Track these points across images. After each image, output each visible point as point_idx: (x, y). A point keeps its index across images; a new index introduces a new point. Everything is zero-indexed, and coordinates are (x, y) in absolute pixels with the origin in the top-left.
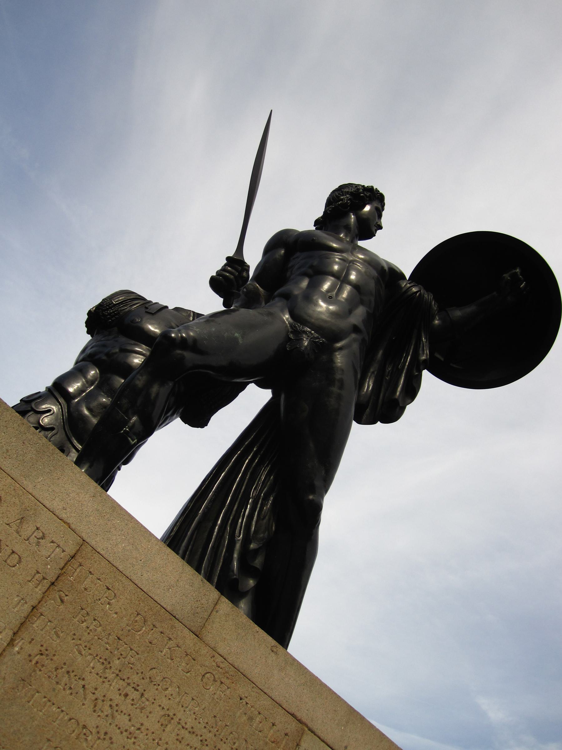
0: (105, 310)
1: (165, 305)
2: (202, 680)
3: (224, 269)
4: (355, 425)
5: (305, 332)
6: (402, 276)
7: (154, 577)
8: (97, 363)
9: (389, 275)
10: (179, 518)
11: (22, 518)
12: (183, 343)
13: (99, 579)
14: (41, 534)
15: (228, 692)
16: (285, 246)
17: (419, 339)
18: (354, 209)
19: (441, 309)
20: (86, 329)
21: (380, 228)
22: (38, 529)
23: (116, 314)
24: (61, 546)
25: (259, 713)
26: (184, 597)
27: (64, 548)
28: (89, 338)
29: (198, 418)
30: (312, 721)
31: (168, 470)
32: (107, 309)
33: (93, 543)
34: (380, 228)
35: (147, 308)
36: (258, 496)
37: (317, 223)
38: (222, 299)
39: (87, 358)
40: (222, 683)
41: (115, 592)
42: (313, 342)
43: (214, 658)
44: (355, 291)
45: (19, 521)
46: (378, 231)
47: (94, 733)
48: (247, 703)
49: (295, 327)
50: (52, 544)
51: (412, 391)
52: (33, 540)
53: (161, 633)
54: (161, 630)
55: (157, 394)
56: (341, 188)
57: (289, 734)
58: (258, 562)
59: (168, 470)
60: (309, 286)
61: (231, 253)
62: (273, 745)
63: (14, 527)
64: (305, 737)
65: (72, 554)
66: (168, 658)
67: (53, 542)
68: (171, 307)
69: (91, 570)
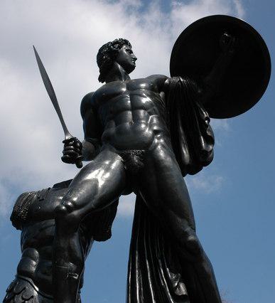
3: (65, 150)
4: (193, 183)
6: (166, 78)
9: (157, 85)
10: (128, 295)
16: (92, 106)
18: (113, 59)
28: (20, 232)
29: (105, 235)
36: (162, 255)
37: (101, 79)
39: (27, 245)
56: (101, 50)
59: (106, 273)
60: (142, 83)
68: (52, 187)
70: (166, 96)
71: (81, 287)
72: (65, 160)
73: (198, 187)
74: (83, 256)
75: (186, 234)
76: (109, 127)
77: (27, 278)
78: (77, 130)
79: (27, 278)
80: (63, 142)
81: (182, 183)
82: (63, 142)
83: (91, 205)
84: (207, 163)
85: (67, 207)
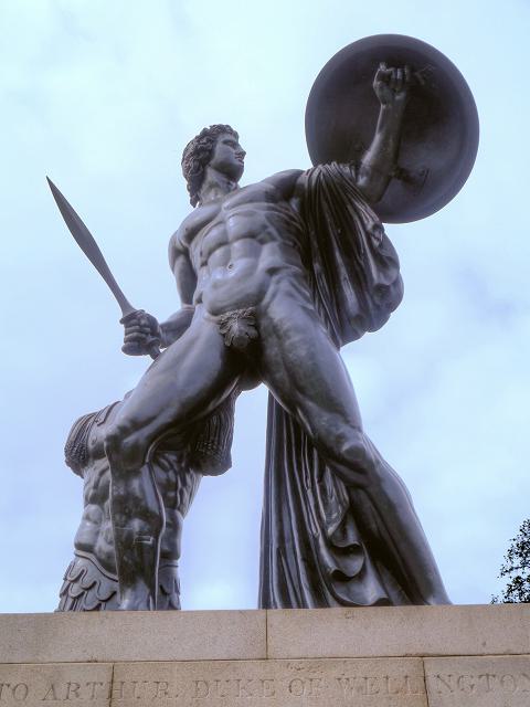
9: (286, 188)
12: (124, 431)
15: (322, 683)
17: (356, 210)
18: (211, 159)
30: (430, 646)
31: (224, 527)
33: (125, 657)
40: (311, 680)
42: (242, 318)
44: (248, 240)
51: (387, 260)
52: (72, 695)
55: (141, 486)
58: (352, 538)
59: (224, 527)
61: (120, 315)
62: (399, 694)
63: (50, 697)
64: (427, 666)
67: (88, 684)
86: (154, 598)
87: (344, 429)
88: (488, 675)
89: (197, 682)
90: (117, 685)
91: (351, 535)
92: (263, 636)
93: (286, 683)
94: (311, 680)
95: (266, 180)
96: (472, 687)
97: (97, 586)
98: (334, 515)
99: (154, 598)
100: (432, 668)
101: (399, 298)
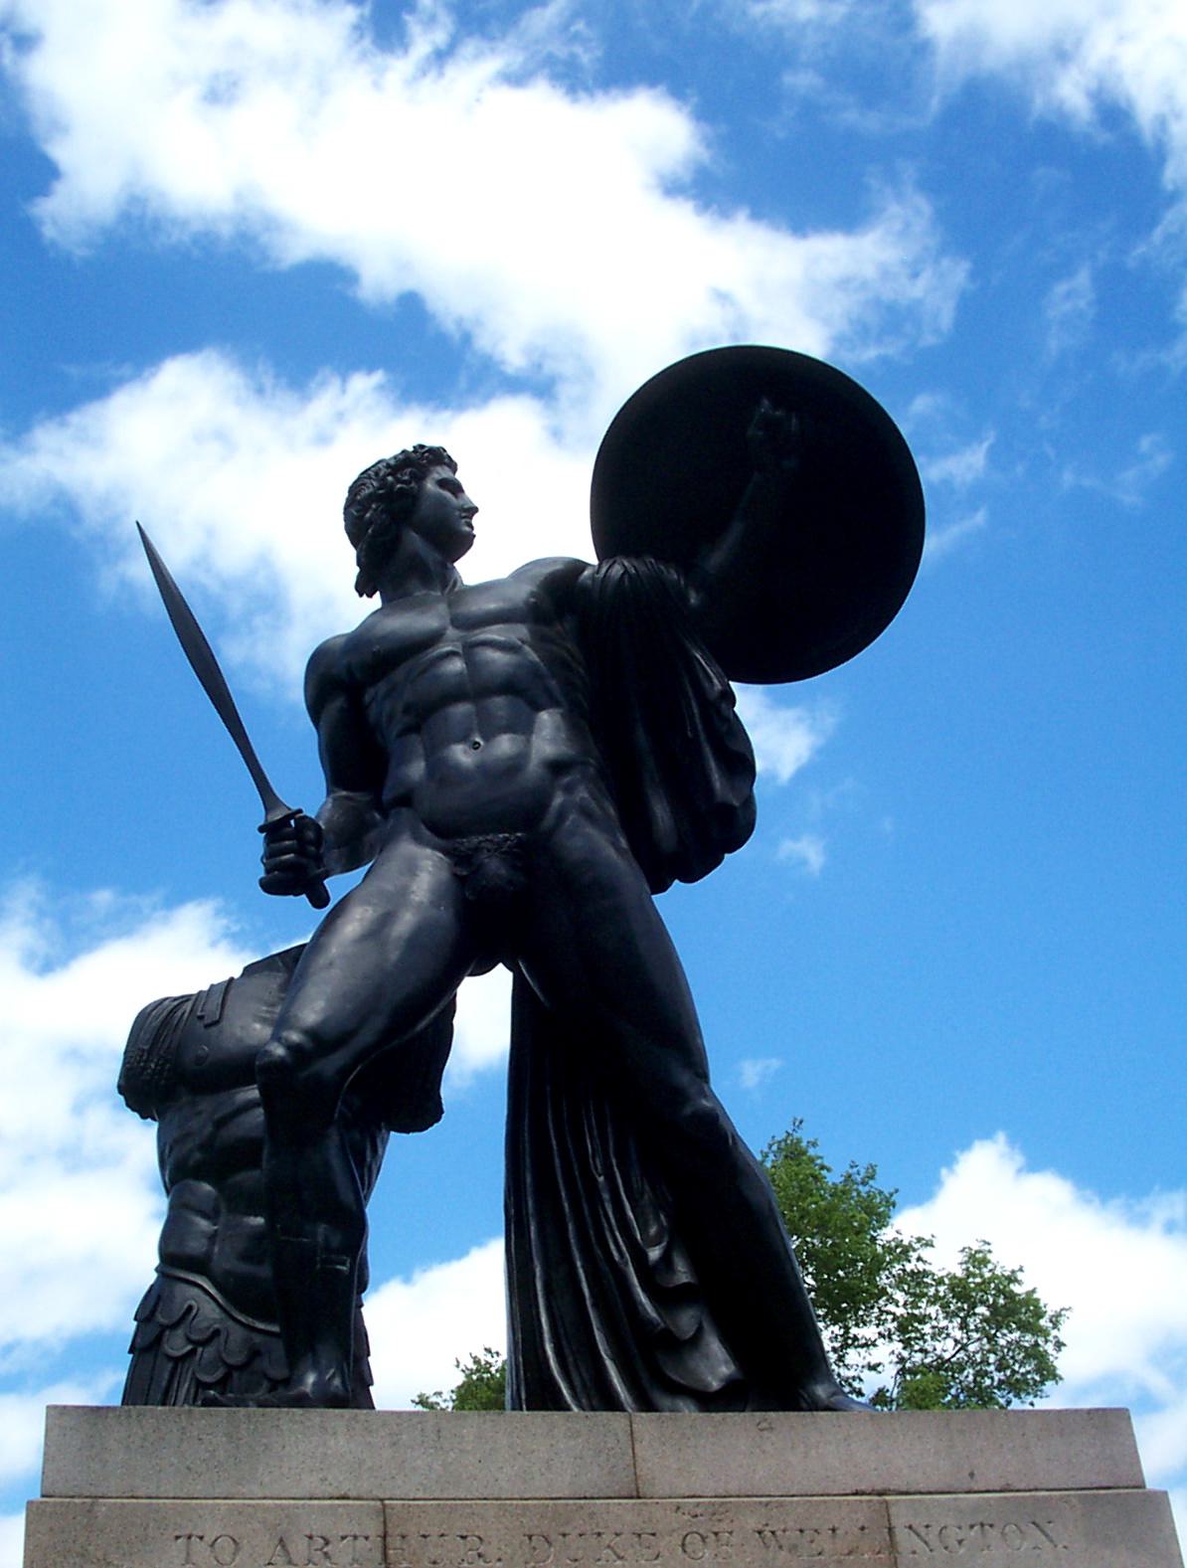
0: (141, 1074)
1: (227, 978)
2: (685, 1551)
3: (270, 855)
4: (679, 907)
5: (477, 849)
7: (516, 1468)
8: (198, 1173)
9: (558, 593)
11: (281, 1540)
13: (442, 1535)
14: (321, 1541)
19: (687, 566)
20: (136, 1115)
21: (474, 510)
22: (311, 1537)
23: (163, 1065)
24: (358, 1533)
25: (801, 1531)
26: (578, 1461)
27: (364, 1534)
32: (144, 1069)
34: (474, 510)
35: (201, 1018)
37: (364, 587)
38: (304, 896)
40: (716, 1534)
41: (477, 1533)
43: (681, 1510)
45: (279, 1548)
46: (476, 520)
47: (696, 1509)
48: (773, 1533)
49: (455, 849)
50: (345, 1541)
53: (581, 1535)
54: (578, 1531)
56: (355, 489)
57: (866, 1526)
61: (259, 816)
65: (381, 1533)
66: (615, 1561)
69: (422, 1533)
70: (845, 1238)
71: (369, 1355)
72: (271, 886)
73: (702, 924)
74: (357, 1193)
75: (679, 1096)
76: (405, 760)
77: (192, 1277)
78: (308, 792)
79: (192, 1277)
80: (261, 829)
81: (651, 900)
82: (261, 829)
83: (367, 1036)
84: (736, 840)
85: (293, 1048)
86: (348, 1364)
87: (684, 1078)
88: (982, 1525)
89: (530, 1537)
90: (394, 1542)
91: (685, 1263)
92: (628, 1459)
93: (677, 1540)
94: (716, 1534)
95: (519, 575)
96: (960, 1542)
97: (222, 1337)
98: (653, 1230)
99: (348, 1364)
100: (902, 1512)
101: (750, 828)
